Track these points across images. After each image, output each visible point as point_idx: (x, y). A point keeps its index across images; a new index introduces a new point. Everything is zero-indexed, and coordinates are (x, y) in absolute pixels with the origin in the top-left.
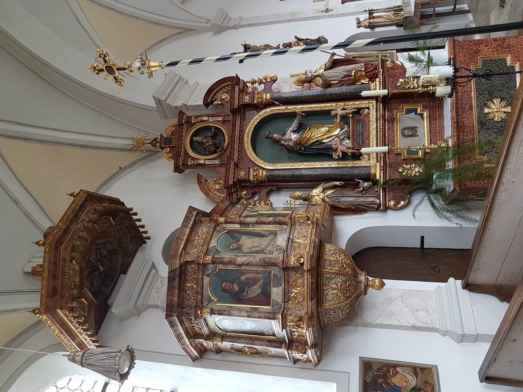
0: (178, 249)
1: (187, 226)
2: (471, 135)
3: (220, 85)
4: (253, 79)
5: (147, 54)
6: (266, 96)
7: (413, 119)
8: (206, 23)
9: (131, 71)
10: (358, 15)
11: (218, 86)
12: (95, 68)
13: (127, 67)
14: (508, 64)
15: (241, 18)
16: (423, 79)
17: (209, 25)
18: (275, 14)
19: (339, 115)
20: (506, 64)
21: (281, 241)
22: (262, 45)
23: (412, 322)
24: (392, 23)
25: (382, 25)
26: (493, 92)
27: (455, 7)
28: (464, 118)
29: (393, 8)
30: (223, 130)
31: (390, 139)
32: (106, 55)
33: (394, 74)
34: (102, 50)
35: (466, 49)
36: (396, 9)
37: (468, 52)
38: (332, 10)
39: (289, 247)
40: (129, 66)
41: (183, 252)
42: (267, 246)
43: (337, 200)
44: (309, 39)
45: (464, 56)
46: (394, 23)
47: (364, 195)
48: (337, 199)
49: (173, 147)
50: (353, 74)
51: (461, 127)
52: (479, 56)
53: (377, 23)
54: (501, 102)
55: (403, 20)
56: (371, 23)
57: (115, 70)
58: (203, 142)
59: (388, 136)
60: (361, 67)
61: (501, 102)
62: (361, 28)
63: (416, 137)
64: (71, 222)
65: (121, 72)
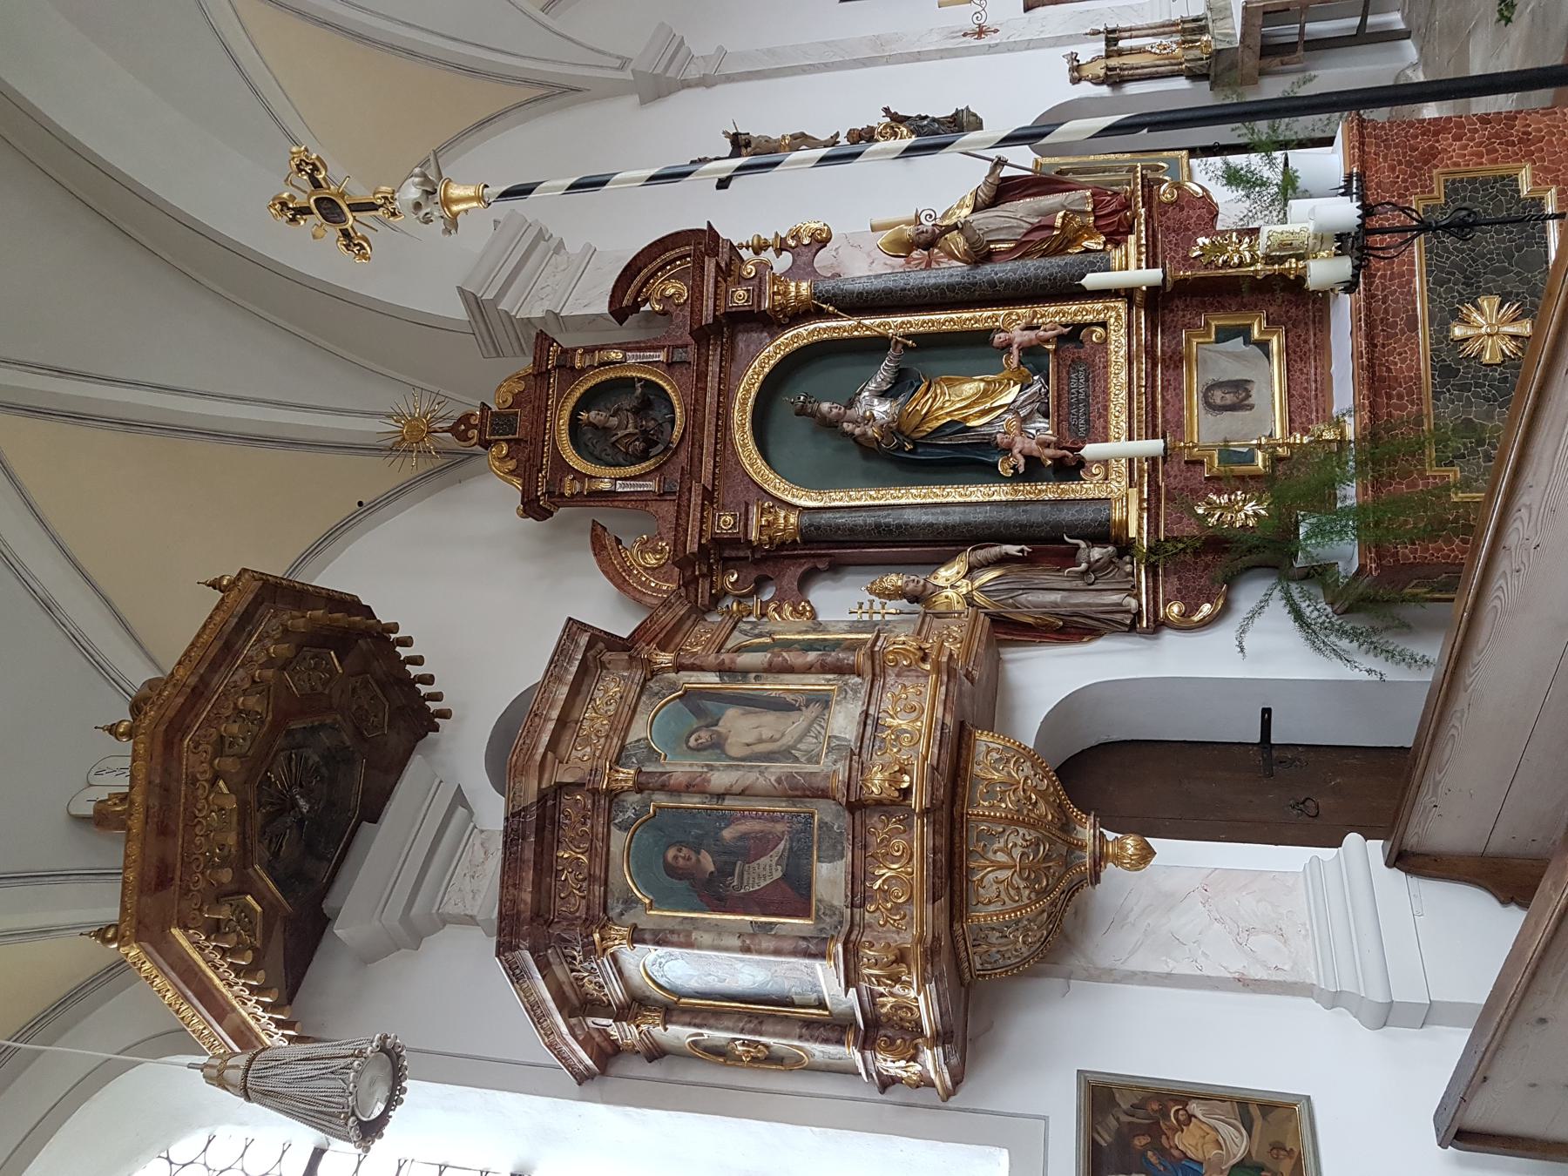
0: (535, 747)
1: (559, 679)
2: (1412, 405)
3: (660, 256)
4: (759, 236)
5: (439, 161)
6: (797, 287)
7: (1237, 357)
8: (617, 69)
9: (394, 214)
10: (1074, 44)
11: (655, 259)
12: (284, 204)
13: (379, 202)
14: (1524, 193)
15: (722, 53)
16: (1268, 238)
17: (627, 75)
18: (825, 43)
19: (1015, 346)
20: (1518, 191)
21: (843, 722)
22: (785, 134)
23: (1235, 965)
24: (1176, 68)
25: (1146, 74)
26: (1477, 275)
27: (1364, 20)
28: (1390, 353)
29: (1178, 25)
30: (670, 391)
31: (1168, 416)
32: (318, 164)
33: (1181, 223)
34: (306, 150)
35: (1396, 146)
36: (1186, 26)
37: (1404, 157)
38: (996, 31)
39: (866, 742)
40: (386, 198)
41: (550, 755)
42: (800, 739)
43: (1011, 601)
44: (926, 117)
45: (1392, 169)
46: (1182, 70)
47: (1092, 584)
48: (1011, 598)
49: (518, 441)
50: (1058, 222)
51: (1382, 380)
52: (1437, 167)
53: (1132, 69)
54: (1501, 306)
55: (1207, 59)
56: (1114, 69)
57: (346, 209)
58: (607, 425)
59: (1163, 408)
60: (1081, 201)
61: (1501, 306)
62: (1084, 83)
63: (1247, 412)
64: (214, 666)
65: (363, 216)
